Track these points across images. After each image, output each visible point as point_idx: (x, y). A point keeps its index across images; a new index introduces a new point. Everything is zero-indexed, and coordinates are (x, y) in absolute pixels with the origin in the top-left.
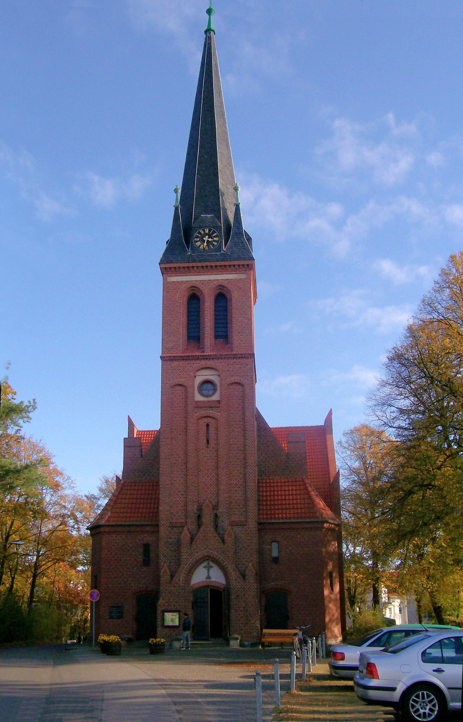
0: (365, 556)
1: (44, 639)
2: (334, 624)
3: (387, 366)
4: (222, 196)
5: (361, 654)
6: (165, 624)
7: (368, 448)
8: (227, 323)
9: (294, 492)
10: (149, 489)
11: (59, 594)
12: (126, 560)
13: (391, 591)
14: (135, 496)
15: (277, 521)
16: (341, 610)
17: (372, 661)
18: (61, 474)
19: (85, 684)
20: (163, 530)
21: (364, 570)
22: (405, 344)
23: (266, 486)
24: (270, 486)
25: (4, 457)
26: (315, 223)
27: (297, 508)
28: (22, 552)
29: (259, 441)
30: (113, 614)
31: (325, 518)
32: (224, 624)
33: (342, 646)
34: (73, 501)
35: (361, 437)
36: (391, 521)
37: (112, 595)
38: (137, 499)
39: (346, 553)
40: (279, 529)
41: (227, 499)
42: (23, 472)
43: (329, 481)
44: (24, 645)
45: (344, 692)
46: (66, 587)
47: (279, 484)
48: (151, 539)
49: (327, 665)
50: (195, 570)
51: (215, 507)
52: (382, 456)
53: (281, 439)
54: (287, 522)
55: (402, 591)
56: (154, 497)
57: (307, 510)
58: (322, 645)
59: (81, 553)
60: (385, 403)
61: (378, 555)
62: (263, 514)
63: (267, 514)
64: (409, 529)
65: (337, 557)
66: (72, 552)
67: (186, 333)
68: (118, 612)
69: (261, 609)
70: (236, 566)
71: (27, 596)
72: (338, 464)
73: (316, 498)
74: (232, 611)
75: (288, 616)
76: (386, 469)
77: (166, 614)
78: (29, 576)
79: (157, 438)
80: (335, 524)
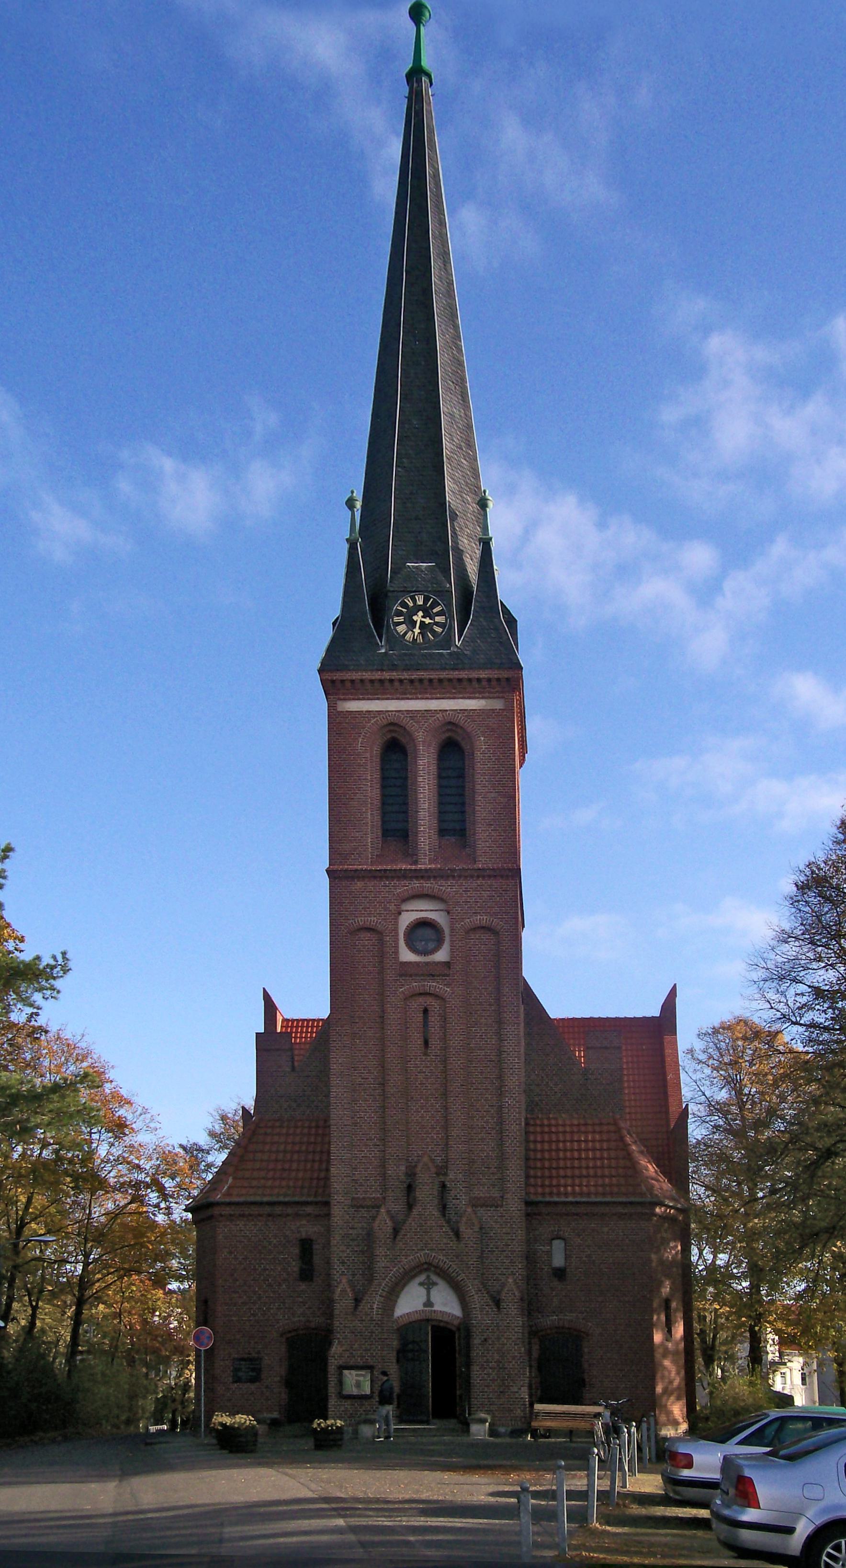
0: (735, 1271)
1: (101, 1425)
2: (672, 1398)
3: (794, 901)
4: (452, 520)
5: (725, 1458)
6: (344, 1393)
7: (747, 1064)
8: (463, 804)
9: (598, 1145)
10: (309, 1134)
11: (132, 1338)
12: (265, 1269)
13: (786, 1342)
14: (282, 1147)
15: (563, 1199)
16: (686, 1373)
17: (747, 1473)
18: (129, 1103)
19: (186, 1511)
20: (339, 1213)
21: (733, 1298)
22: (834, 857)
23: (542, 1133)
24: (550, 1132)
25: (6, 1068)
26: (655, 588)
27: (603, 1176)
28: (53, 1257)
29: (528, 1044)
30: (240, 1374)
31: (657, 1195)
32: (458, 1393)
33: (689, 1441)
34: (155, 1156)
35: (734, 1041)
36: (788, 1206)
37: (238, 1337)
38: (285, 1152)
39: (697, 1264)
40: (567, 1215)
41: (464, 1155)
42: (48, 1099)
43: (668, 1125)
44: (60, 1438)
45: (691, 1529)
46: (145, 1322)
47: (568, 1129)
48: (315, 1229)
49: (659, 1477)
50: (402, 1289)
51: (442, 1170)
52: (775, 1081)
53: (572, 1041)
54: (584, 1202)
55: (808, 1341)
56: (318, 1149)
57: (622, 1181)
58: (649, 1437)
59: (174, 1256)
60: (785, 976)
61: (762, 1270)
62: (535, 1186)
63: (543, 1186)
64: (823, 1224)
65: (680, 1272)
66: (156, 1255)
67: (380, 823)
68: (250, 1369)
69: (531, 1366)
70: (482, 1283)
71: (65, 1341)
72: (686, 1092)
73: (641, 1158)
74: (475, 1368)
75: (584, 1380)
76: (782, 1107)
77: (346, 1372)
78: (69, 1302)
79: (323, 1032)
80: (676, 1209)
